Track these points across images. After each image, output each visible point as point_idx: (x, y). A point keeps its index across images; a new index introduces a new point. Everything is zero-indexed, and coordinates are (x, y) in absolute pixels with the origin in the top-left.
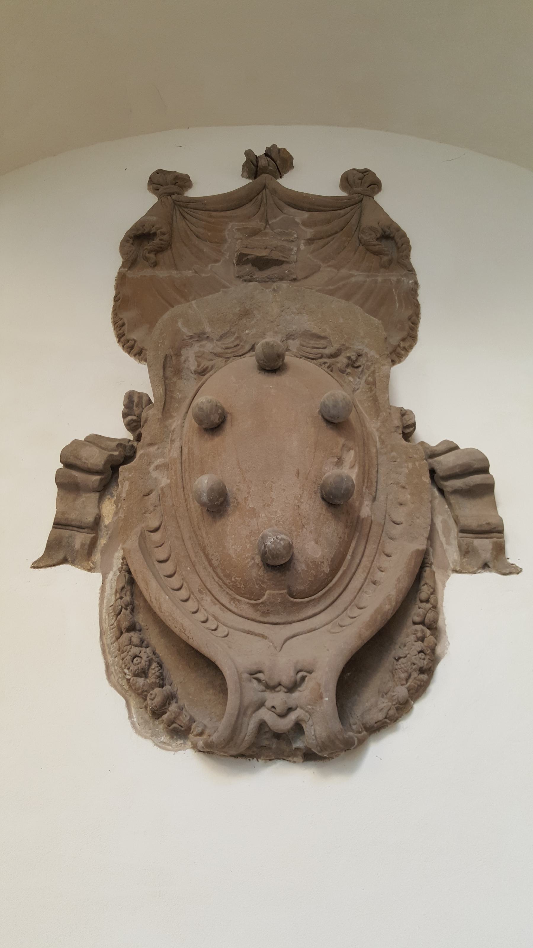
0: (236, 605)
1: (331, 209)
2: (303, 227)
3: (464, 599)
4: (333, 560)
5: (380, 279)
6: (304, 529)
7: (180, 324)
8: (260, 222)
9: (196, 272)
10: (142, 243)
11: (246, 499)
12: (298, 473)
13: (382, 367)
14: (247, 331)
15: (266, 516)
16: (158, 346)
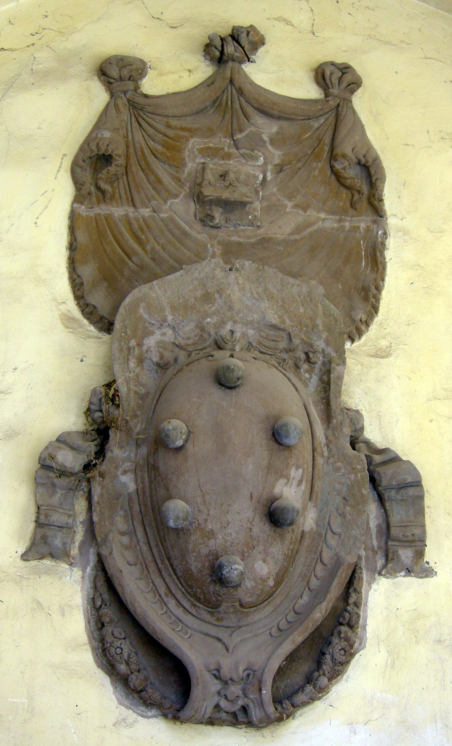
0: (196, 610)
1: (302, 118)
2: (270, 148)
3: (384, 599)
4: (277, 575)
5: (347, 225)
6: (254, 550)
7: (141, 311)
8: (224, 138)
9: (154, 211)
10: (96, 167)
11: (206, 520)
12: (252, 497)
13: (337, 367)
14: (209, 320)
15: (223, 538)
16: (121, 336)
